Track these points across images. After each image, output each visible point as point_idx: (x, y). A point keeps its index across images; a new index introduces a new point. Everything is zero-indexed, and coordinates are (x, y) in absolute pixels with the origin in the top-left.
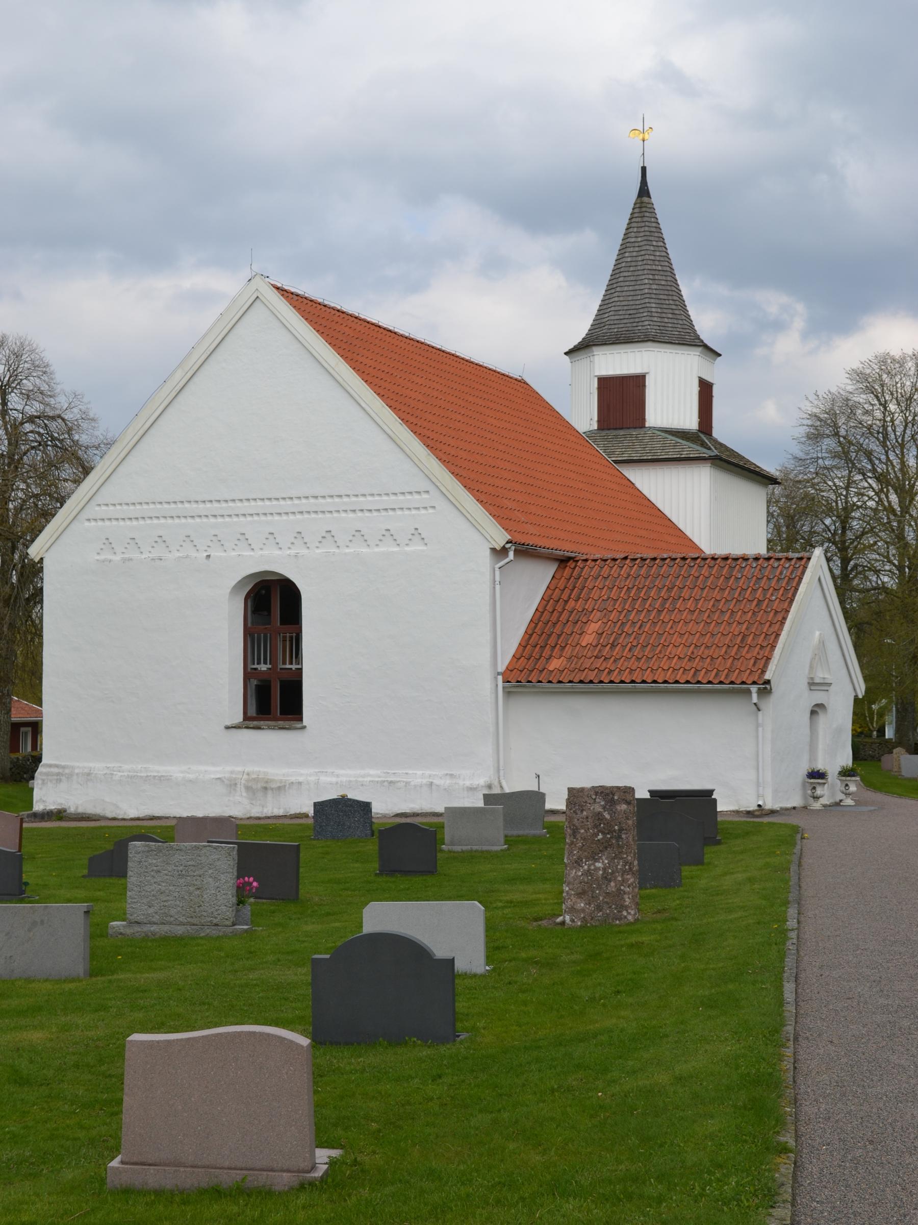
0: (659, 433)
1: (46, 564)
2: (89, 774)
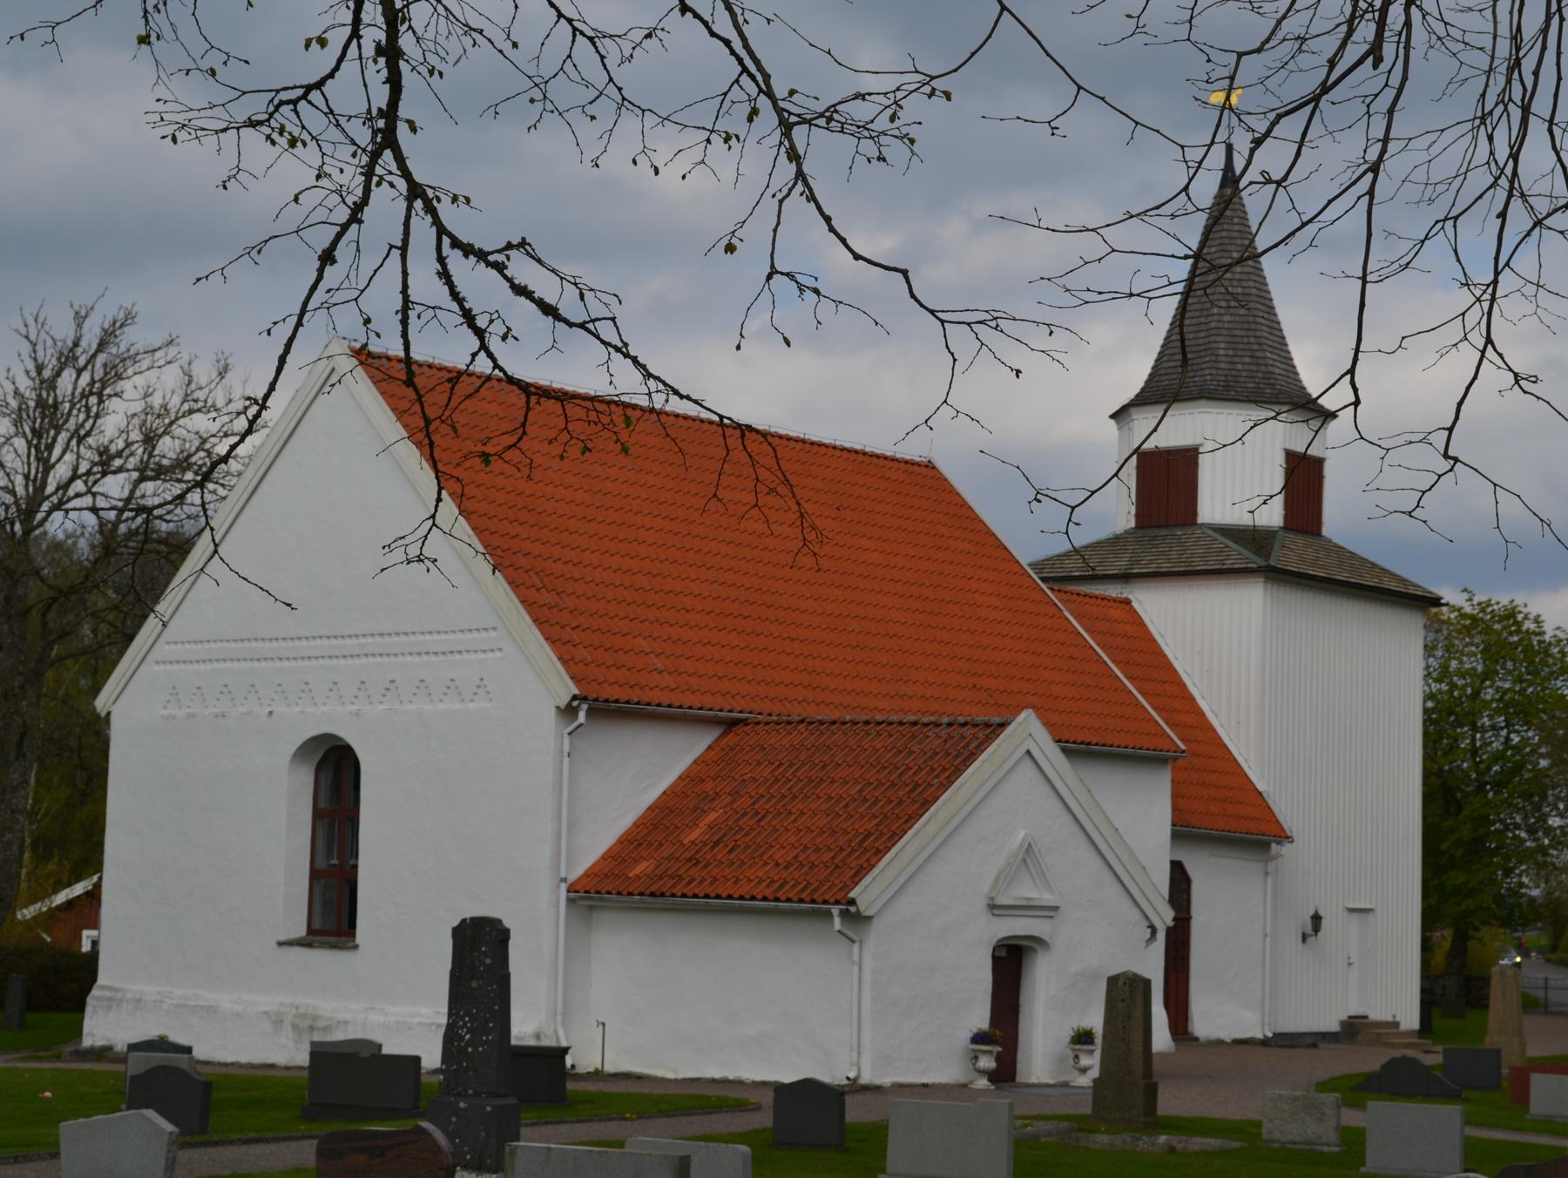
0: (1210, 532)
1: (114, 719)
2: (139, 1001)
